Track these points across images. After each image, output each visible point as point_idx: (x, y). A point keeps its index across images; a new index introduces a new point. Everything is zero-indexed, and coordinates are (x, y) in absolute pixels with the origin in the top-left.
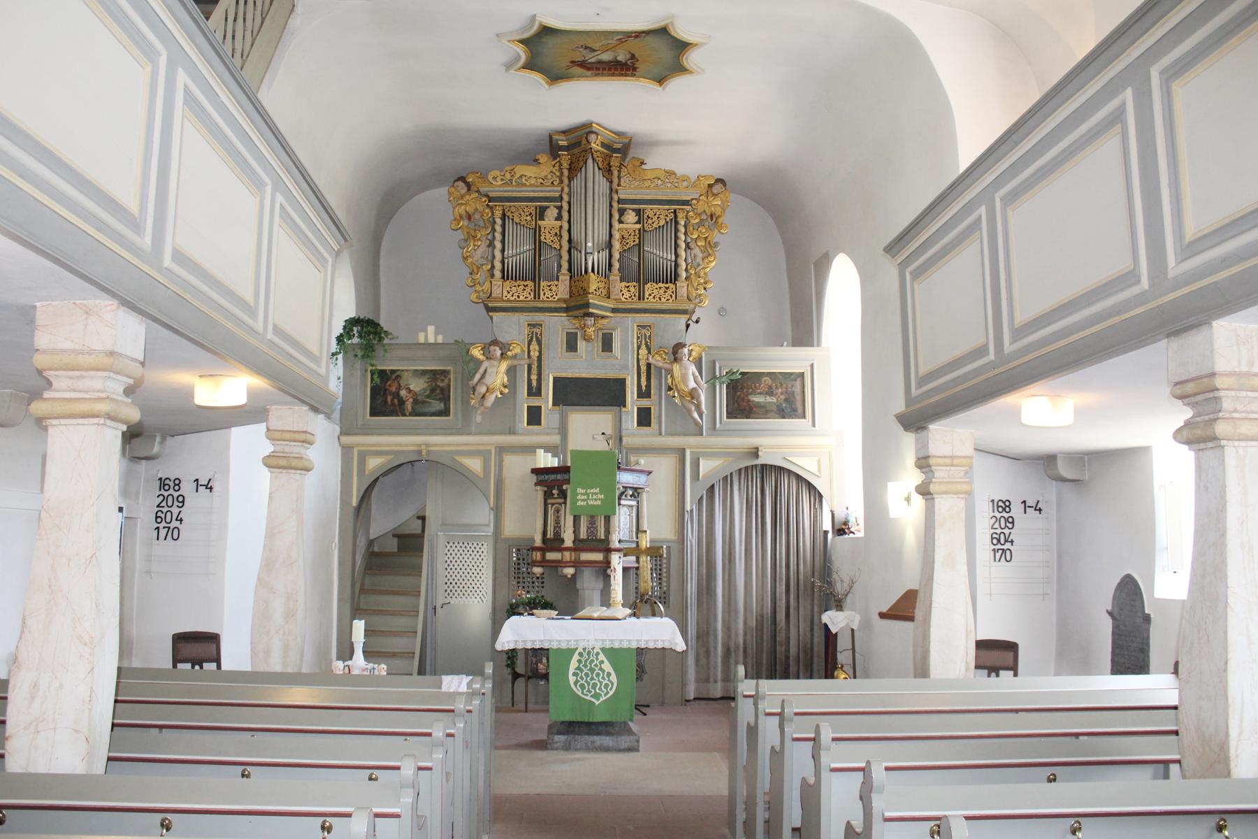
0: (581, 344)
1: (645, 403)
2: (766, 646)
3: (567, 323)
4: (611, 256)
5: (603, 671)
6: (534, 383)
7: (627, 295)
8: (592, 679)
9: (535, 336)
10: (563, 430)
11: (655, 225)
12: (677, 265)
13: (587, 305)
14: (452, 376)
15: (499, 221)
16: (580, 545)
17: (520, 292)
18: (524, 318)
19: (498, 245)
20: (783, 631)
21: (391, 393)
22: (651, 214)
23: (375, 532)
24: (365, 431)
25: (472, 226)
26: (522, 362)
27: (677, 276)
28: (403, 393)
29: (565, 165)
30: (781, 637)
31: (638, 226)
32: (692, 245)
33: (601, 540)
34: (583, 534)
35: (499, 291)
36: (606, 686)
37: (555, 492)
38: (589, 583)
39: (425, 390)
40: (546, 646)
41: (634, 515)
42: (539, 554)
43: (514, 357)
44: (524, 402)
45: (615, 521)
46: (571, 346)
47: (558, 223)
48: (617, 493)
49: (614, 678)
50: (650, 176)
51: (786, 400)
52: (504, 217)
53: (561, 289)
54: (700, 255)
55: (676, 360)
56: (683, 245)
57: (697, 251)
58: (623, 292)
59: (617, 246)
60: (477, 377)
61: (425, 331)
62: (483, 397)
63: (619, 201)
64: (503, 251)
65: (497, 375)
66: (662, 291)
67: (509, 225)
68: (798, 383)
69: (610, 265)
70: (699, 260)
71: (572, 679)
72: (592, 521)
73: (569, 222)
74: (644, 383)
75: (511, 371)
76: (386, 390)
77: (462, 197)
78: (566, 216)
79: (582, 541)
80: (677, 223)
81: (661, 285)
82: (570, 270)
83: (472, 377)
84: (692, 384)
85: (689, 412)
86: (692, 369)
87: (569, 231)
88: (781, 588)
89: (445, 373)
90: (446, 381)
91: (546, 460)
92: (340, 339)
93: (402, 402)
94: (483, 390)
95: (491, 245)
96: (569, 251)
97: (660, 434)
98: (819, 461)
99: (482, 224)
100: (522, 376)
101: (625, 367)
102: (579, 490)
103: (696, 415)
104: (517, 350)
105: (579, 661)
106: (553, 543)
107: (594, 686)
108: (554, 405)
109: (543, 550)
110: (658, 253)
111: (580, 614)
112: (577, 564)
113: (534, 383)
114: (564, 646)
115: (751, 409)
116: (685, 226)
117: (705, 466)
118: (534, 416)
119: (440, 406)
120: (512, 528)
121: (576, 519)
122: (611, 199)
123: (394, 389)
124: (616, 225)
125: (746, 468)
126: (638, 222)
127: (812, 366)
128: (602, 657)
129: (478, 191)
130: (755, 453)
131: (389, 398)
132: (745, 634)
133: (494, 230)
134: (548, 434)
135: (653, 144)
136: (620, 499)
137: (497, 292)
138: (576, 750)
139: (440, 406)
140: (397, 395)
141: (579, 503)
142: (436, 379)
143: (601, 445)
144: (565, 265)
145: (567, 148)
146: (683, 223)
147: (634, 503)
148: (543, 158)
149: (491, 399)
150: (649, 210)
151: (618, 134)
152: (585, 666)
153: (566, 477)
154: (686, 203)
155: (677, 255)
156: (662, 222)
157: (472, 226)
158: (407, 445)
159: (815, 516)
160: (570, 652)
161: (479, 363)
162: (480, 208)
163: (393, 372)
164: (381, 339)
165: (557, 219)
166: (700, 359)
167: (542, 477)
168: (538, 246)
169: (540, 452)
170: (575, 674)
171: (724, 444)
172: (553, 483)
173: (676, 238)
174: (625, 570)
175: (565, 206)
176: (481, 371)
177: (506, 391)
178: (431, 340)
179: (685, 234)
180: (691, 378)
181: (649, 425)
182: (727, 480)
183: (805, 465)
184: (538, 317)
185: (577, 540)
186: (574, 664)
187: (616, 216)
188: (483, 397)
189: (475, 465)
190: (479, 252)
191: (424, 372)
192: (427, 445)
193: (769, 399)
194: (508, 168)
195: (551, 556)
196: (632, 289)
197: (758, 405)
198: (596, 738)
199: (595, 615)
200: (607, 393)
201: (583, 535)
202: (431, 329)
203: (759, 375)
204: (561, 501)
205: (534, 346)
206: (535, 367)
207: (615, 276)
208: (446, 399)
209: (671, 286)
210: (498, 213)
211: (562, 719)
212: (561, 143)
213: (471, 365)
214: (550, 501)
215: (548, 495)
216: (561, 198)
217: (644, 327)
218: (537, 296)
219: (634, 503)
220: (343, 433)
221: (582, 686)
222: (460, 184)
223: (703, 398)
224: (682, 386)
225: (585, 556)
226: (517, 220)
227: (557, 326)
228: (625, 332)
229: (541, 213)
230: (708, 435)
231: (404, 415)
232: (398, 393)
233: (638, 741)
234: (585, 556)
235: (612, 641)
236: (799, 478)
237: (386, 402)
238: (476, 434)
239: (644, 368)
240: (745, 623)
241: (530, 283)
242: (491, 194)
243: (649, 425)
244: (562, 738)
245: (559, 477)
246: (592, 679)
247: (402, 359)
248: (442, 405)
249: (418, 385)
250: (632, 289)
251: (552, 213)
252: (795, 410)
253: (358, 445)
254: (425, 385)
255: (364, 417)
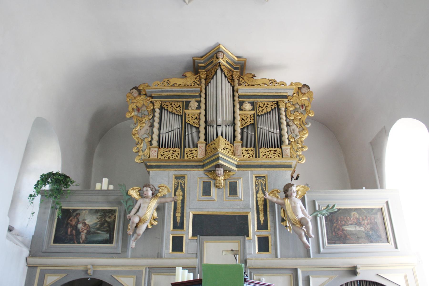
0: (214, 190)
1: (263, 233)
3: (204, 176)
4: (234, 131)
6: (178, 219)
9: (180, 185)
10: (200, 254)
11: (265, 111)
12: (281, 136)
13: (218, 158)
14: (117, 214)
15: (158, 110)
17: (173, 155)
19: (156, 125)
21: (71, 226)
24: (48, 254)
25: (140, 115)
27: (282, 142)
28: (80, 226)
29: (203, 77)
31: (253, 112)
32: (291, 123)
35: (156, 154)
39: (96, 224)
43: (164, 196)
44: (169, 233)
46: (207, 191)
47: (198, 111)
51: (372, 229)
52: (161, 108)
53: (200, 152)
54: (297, 130)
55: (287, 196)
56: (285, 123)
57: (294, 127)
60: (134, 211)
61: (101, 182)
62: (136, 227)
64: (160, 129)
65: (149, 210)
66: (272, 153)
68: (379, 215)
69: (234, 137)
75: (160, 209)
76: (68, 223)
77: (135, 98)
78: (203, 106)
80: (279, 109)
81: (271, 149)
82: (206, 140)
83: (129, 213)
84: (301, 215)
85: (300, 236)
86: (299, 203)
87: (205, 116)
89: (112, 212)
90: (113, 217)
92: (37, 185)
93: (78, 233)
94: (136, 220)
95: (152, 126)
96: (205, 128)
97: (277, 257)
100: (169, 214)
103: (305, 239)
104: (165, 192)
108: (193, 235)
110: (267, 128)
113: (178, 219)
115: (346, 236)
116: (285, 111)
118: (178, 244)
119: (107, 236)
122: (234, 96)
123: (74, 223)
124: (238, 112)
126: (253, 109)
127: (387, 203)
129: (146, 95)
130: (353, 271)
131: (69, 230)
133: (154, 116)
139: (107, 236)
140: (75, 227)
142: (105, 216)
145: (204, 68)
146: (283, 109)
148: (189, 75)
151: (238, 57)
154: (286, 97)
155: (281, 129)
156: (269, 110)
157: (140, 115)
158: (78, 266)
163: (75, 210)
165: (197, 108)
168: (185, 125)
173: (280, 119)
176: (137, 207)
177: (156, 223)
178: (105, 187)
181: (268, 251)
184: (181, 172)
187: (238, 106)
188: (137, 224)
191: (97, 211)
192: (94, 266)
193: (358, 228)
196: (251, 152)
197: (351, 233)
202: (105, 181)
203: (347, 212)
206: (179, 206)
208: (111, 231)
209: (279, 149)
210: (157, 105)
212: (200, 65)
213: (130, 203)
216: (200, 96)
217: (260, 178)
218: (182, 155)
220: (32, 254)
222: (135, 91)
223: (310, 225)
226: (170, 110)
227: (195, 178)
228: (247, 183)
229: (187, 105)
231: (79, 243)
232: (76, 227)
238: (133, 257)
239: (261, 207)
241: (177, 149)
242: (153, 94)
243: (268, 251)
248: (108, 235)
250: (251, 152)
251: (194, 104)
252: (379, 236)
255: (49, 243)
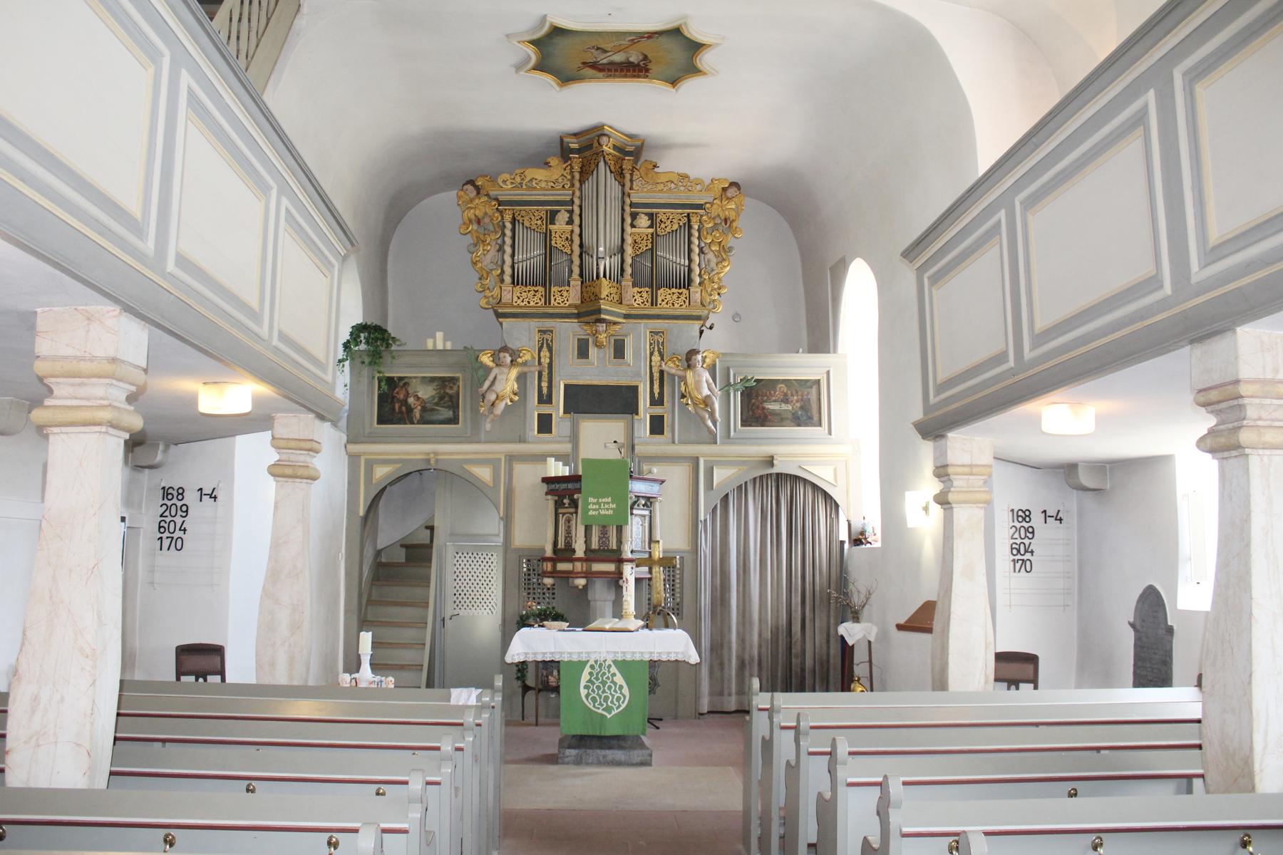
0: (593, 351)
1: (658, 411)
2: (781, 658)
3: (578, 329)
4: (623, 261)
5: (615, 684)
6: (545, 391)
7: (640, 300)
8: (604, 692)
9: (546, 342)
10: (574, 439)
11: (668, 230)
12: (690, 270)
13: (599, 311)
14: (461, 384)
15: (509, 225)
16: (591, 555)
18: (535, 324)
19: (508, 250)
20: (799, 643)
21: (399, 401)
22: (664, 218)
23: (382, 542)
24: (372, 439)
25: (481, 230)
26: (533, 369)
27: (690, 281)
28: (411, 400)
29: (577, 168)
30: (796, 649)
31: (651, 230)
32: (706, 250)
33: (613, 551)
34: (595, 545)
35: (509, 296)
36: (618, 699)
37: (566, 501)
38: (601, 594)
39: (433, 397)
40: (557, 658)
41: (647, 525)
42: (549, 565)
43: (525, 364)
44: (534, 410)
45: (627, 531)
46: (583, 352)
47: (570, 227)
48: (630, 503)
49: (626, 691)
50: (663, 179)
51: (802, 408)
52: (514, 221)
53: (573, 295)
54: (714, 260)
55: (689, 367)
56: (697, 250)
57: (710, 256)
58: (636, 297)
59: (629, 250)
60: (487, 384)
61: (434, 337)
62: (493, 404)
63: (632, 205)
64: (513, 256)
65: (507, 382)
66: (675, 297)
67: (519, 229)
68: (814, 390)
69: (623, 270)
70: (713, 264)
71: (583, 692)
72: (604, 531)
73: (581, 226)
74: (656, 390)
75: (521, 378)
76: (393, 397)
77: (471, 201)
78: (577, 220)
79: (593, 551)
80: (690, 227)
81: (674, 290)
82: (581, 275)
83: (482, 385)
84: (706, 392)
85: (703, 420)
86: (706, 376)
87: (581, 235)
88: (797, 599)
89: (453, 380)
90: (455, 388)
91: (557, 469)
92: (346, 346)
93: (410, 410)
94: (492, 397)
95: (501, 249)
96: (581, 256)
97: (673, 442)
98: (835, 470)
99: (491, 228)
100: (532, 383)
101: (638, 374)
102: (591, 500)
103: (710, 423)
104: (528, 357)
105: (591, 674)
106: (564, 553)
107: (606, 699)
108: (565, 412)
109: (554, 561)
110: (671, 258)
111: (592, 626)
112: (589, 575)
113: (545, 391)
114: (575, 658)
115: (766, 417)
116: (699, 230)
117: (719, 475)
118: (545, 424)
119: (449, 414)
120: (522, 538)
121: (588, 529)
122: (623, 202)
123: (402, 396)
124: (628, 229)
125: (761, 477)
126: (651, 226)
127: (828, 373)
128: (614, 669)
129: (487, 195)
130: (770, 461)
131: (397, 406)
132: (760, 646)
133: (504, 234)
134: (559, 442)
135: (666, 146)
136: (632, 508)
137: (506, 297)
138: (587, 764)
139: (449, 414)
140: (405, 402)
141: (591, 513)
142: (445, 387)
143: (613, 454)
144: (576, 270)
145: (578, 151)
146: (696, 227)
147: (647, 513)
148: (554, 162)
149: (501, 407)
150: (662, 214)
151: (630, 136)
152: (597, 679)
153: (577, 486)
154: (700, 207)
155: (690, 260)
156: (675, 227)
157: (481, 230)
158: (415, 454)
159: (831, 526)
160: (582, 664)
161: (489, 370)
162: (490, 212)
163: (401, 379)
164: (388, 346)
165: (568, 223)
166: (714, 366)
167: (553, 486)
168: (549, 251)
169: (551, 461)
170: (586, 687)
171: (738, 452)
172: (564, 492)
173: (690, 242)
174: (638, 580)
175: (577, 210)
176: (491, 378)
177: (516, 398)
178: (440, 346)
179: (699, 238)
180: (705, 385)
181: (662, 433)
182: (741, 489)
183: (821, 474)
184: (548, 323)
185: (588, 550)
186: (585, 677)
187: (628, 220)
188: (493, 404)
189: (484, 473)
190: (489, 257)
191: (432, 380)
192: (436, 454)
193: (784, 407)
194: (518, 171)
195: (562, 566)
196: (645, 295)
197: (773, 413)
198: (608, 752)
199: (607, 627)
200: (619, 401)
201: (595, 545)
202: (439, 335)
203: (774, 382)
204: (572, 510)
205: (545, 353)
206: (545, 374)
207: (627, 281)
208: (454, 406)
209: (684, 291)
210: (508, 217)
211: (573, 732)
212: (572, 146)
213: (481, 372)
214: (560, 511)
215: (559, 504)
216: (572, 202)
217: (657, 333)
218: (547, 302)
219: (647, 513)
220: (350, 441)
221: (594, 700)
222: (470, 187)
223: (717, 406)
224: (696, 394)
225: (597, 567)
226: (527, 224)
227: (568, 332)
228: (638, 338)
229: (552, 217)
230: (722, 443)
231: (412, 423)
232: (406, 401)
233: (651, 755)
234: (597, 567)
235: (624, 653)
236: (815, 487)
237: (394, 409)
238: (486, 442)
239: (656, 375)
240: (760, 635)
241: (541, 289)
242: (501, 198)
243: (662, 433)
244: (573, 752)
245: (570, 486)
246: (604, 692)
247: (410, 366)
248: (451, 413)
249: (426, 392)
250: (645, 295)
251: (563, 217)
252: (810, 418)
253: (365, 453)
254: (434, 393)
255: (371, 424)
